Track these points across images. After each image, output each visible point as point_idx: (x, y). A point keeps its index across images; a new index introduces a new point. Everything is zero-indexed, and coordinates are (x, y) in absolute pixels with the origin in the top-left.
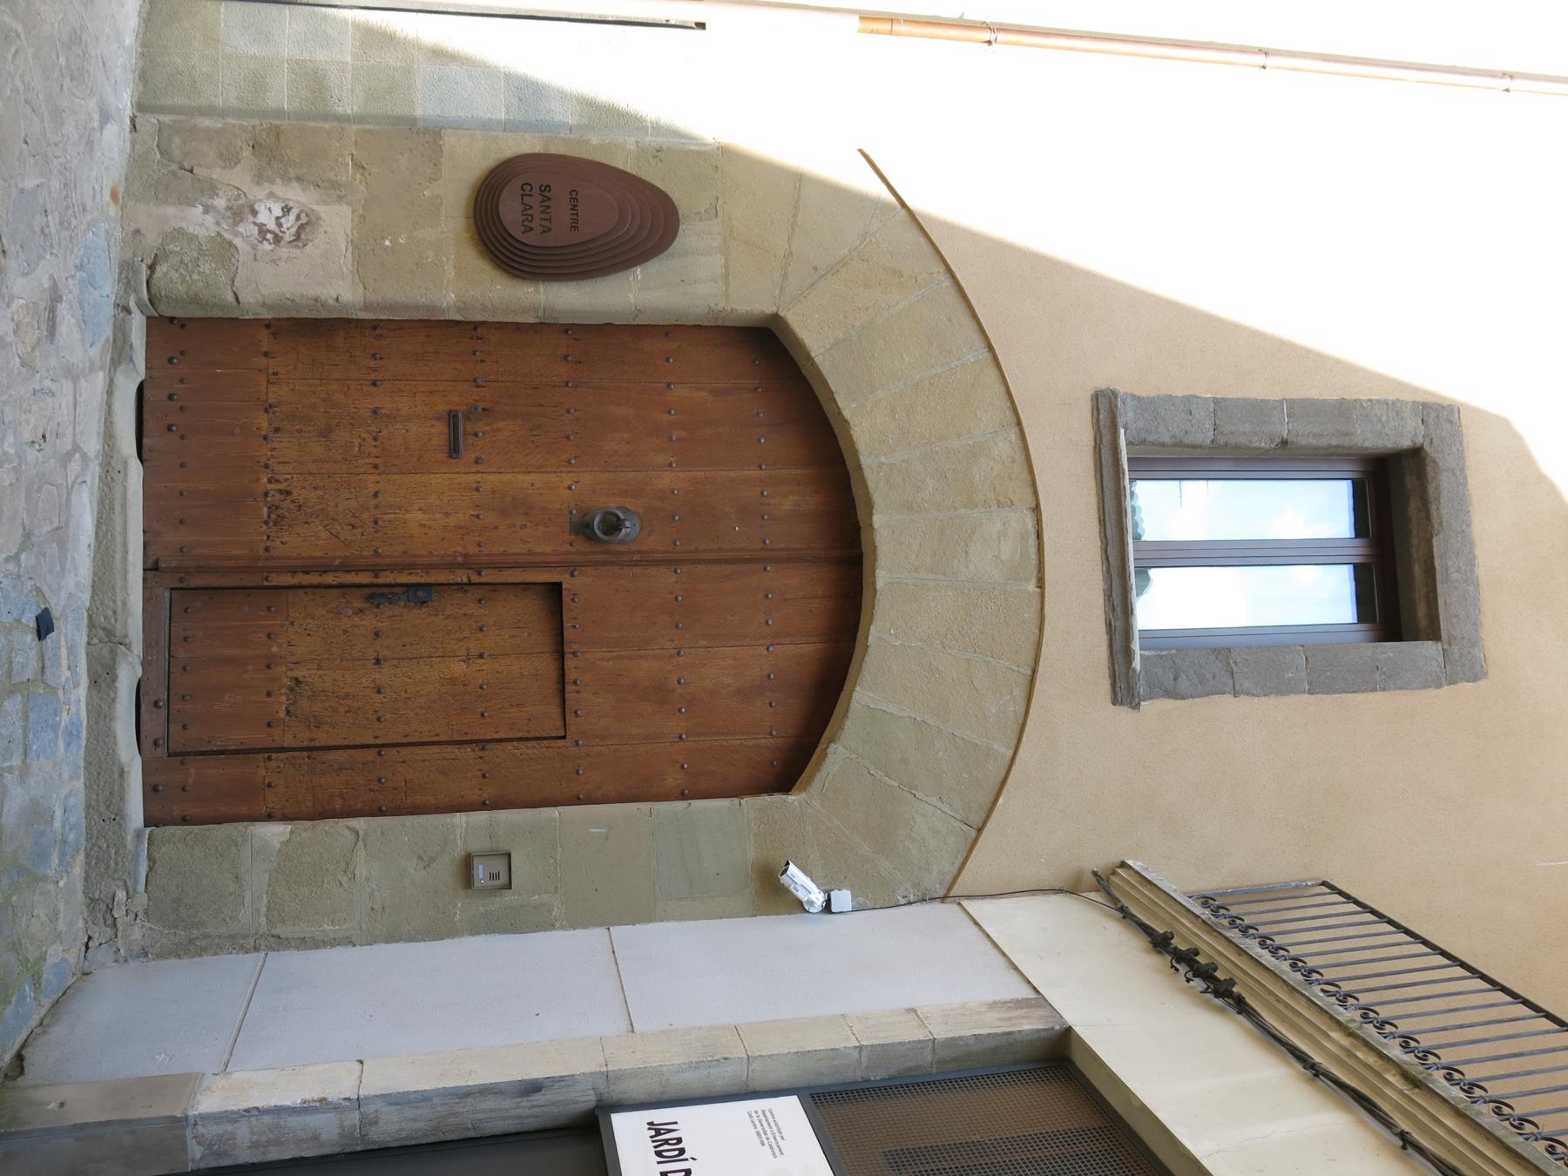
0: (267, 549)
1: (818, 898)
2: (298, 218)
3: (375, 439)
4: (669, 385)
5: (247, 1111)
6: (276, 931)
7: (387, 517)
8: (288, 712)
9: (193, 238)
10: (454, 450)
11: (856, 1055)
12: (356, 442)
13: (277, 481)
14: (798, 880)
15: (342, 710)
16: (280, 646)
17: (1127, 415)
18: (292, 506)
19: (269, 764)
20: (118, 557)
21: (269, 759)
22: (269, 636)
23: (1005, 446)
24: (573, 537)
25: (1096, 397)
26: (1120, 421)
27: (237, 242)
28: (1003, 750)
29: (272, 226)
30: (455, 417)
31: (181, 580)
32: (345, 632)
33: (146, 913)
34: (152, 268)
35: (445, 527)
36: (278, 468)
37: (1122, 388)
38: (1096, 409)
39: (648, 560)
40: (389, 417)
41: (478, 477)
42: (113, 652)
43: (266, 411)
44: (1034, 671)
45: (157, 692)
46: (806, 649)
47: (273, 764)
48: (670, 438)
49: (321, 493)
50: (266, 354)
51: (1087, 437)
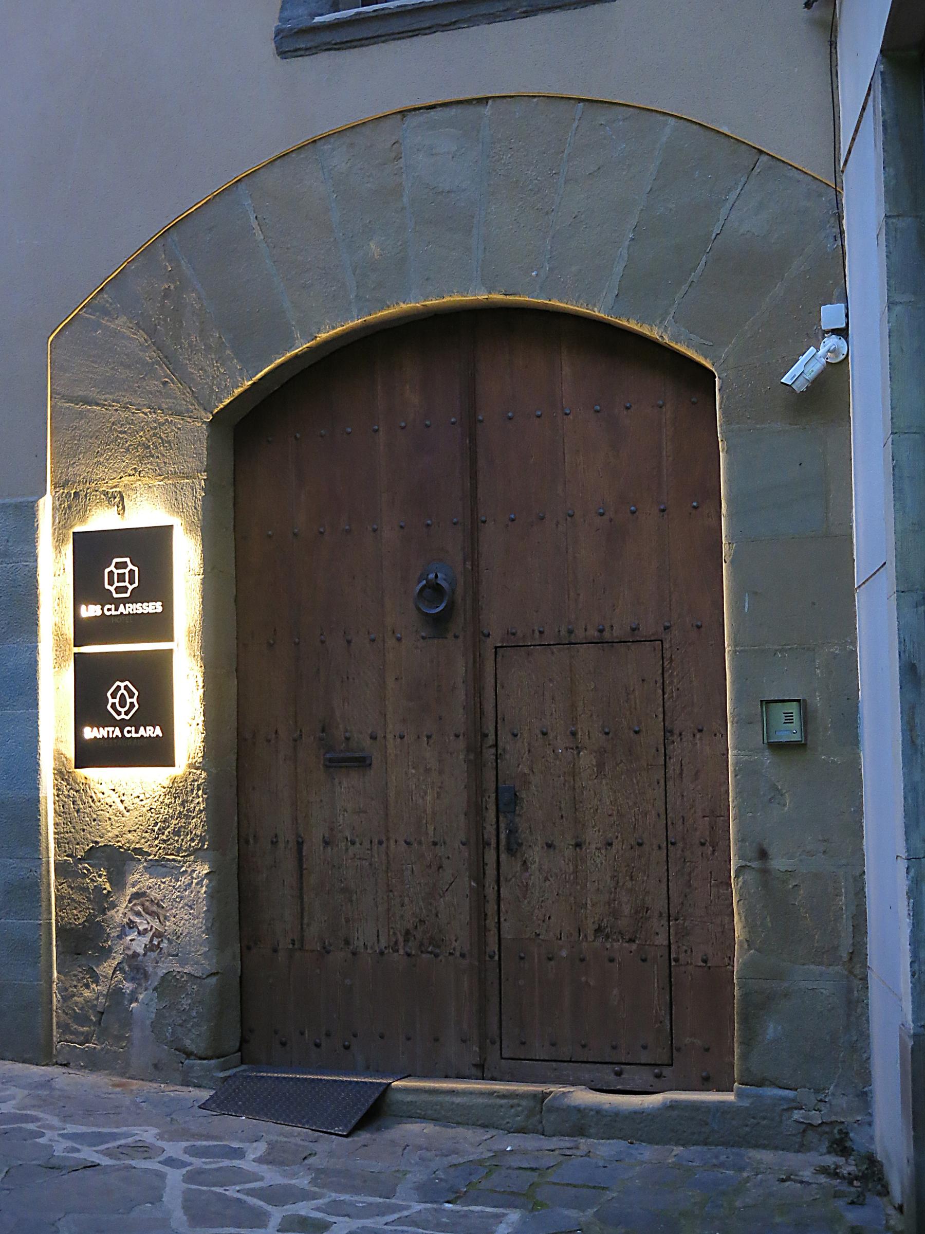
0: (463, 956)
1: (831, 342)
2: (138, 914)
3: (353, 843)
4: (295, 535)
5: (913, 975)
6: (845, 957)
7: (431, 832)
8: (632, 940)
9: (160, 1014)
10: (362, 763)
11: (898, 309)
12: (358, 863)
13: (396, 943)
14: (803, 370)
15: (629, 884)
16: (561, 948)
17: (301, 16)
18: (420, 929)
19: (682, 961)
20: (458, 1100)
21: (676, 960)
22: (550, 959)
23: (338, 158)
24: (450, 636)
25: (283, 54)
26: (305, 23)
27: (162, 972)
28: (668, 130)
29: (145, 940)
30: (330, 760)
31: (493, 1043)
32: (546, 879)
33: (817, 1091)
34: (189, 1055)
35: (441, 772)
36: (383, 942)
37: (274, 23)
38: (296, 53)
39: (473, 554)
40: (332, 829)
41: (390, 737)
42: (550, 1110)
43: (328, 952)
44: (580, 100)
45: (607, 1075)
46: (567, 370)
47: (682, 957)
48: (348, 532)
49: (406, 900)
50: (275, 951)
51: (324, 60)
